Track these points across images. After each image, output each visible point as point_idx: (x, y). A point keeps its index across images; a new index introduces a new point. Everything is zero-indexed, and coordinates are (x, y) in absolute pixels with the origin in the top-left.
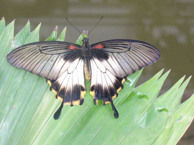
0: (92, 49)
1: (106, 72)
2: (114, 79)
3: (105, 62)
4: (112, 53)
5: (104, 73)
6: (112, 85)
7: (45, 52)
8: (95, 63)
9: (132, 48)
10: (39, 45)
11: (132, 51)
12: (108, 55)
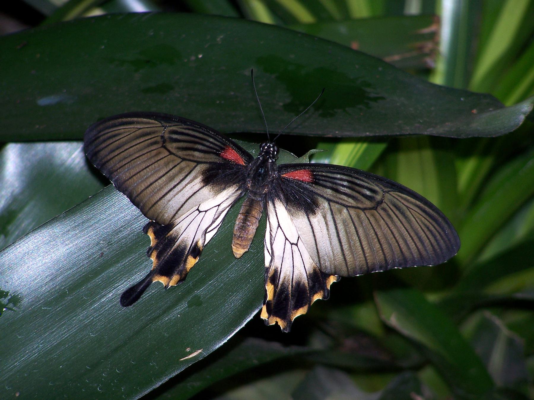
0: (279, 176)
1: (297, 245)
2: (310, 264)
3: (302, 220)
4: (329, 201)
5: (292, 244)
6: (305, 280)
7: (172, 146)
8: (280, 214)
9: (384, 205)
10: (165, 124)
11: (381, 212)
12: (317, 205)
